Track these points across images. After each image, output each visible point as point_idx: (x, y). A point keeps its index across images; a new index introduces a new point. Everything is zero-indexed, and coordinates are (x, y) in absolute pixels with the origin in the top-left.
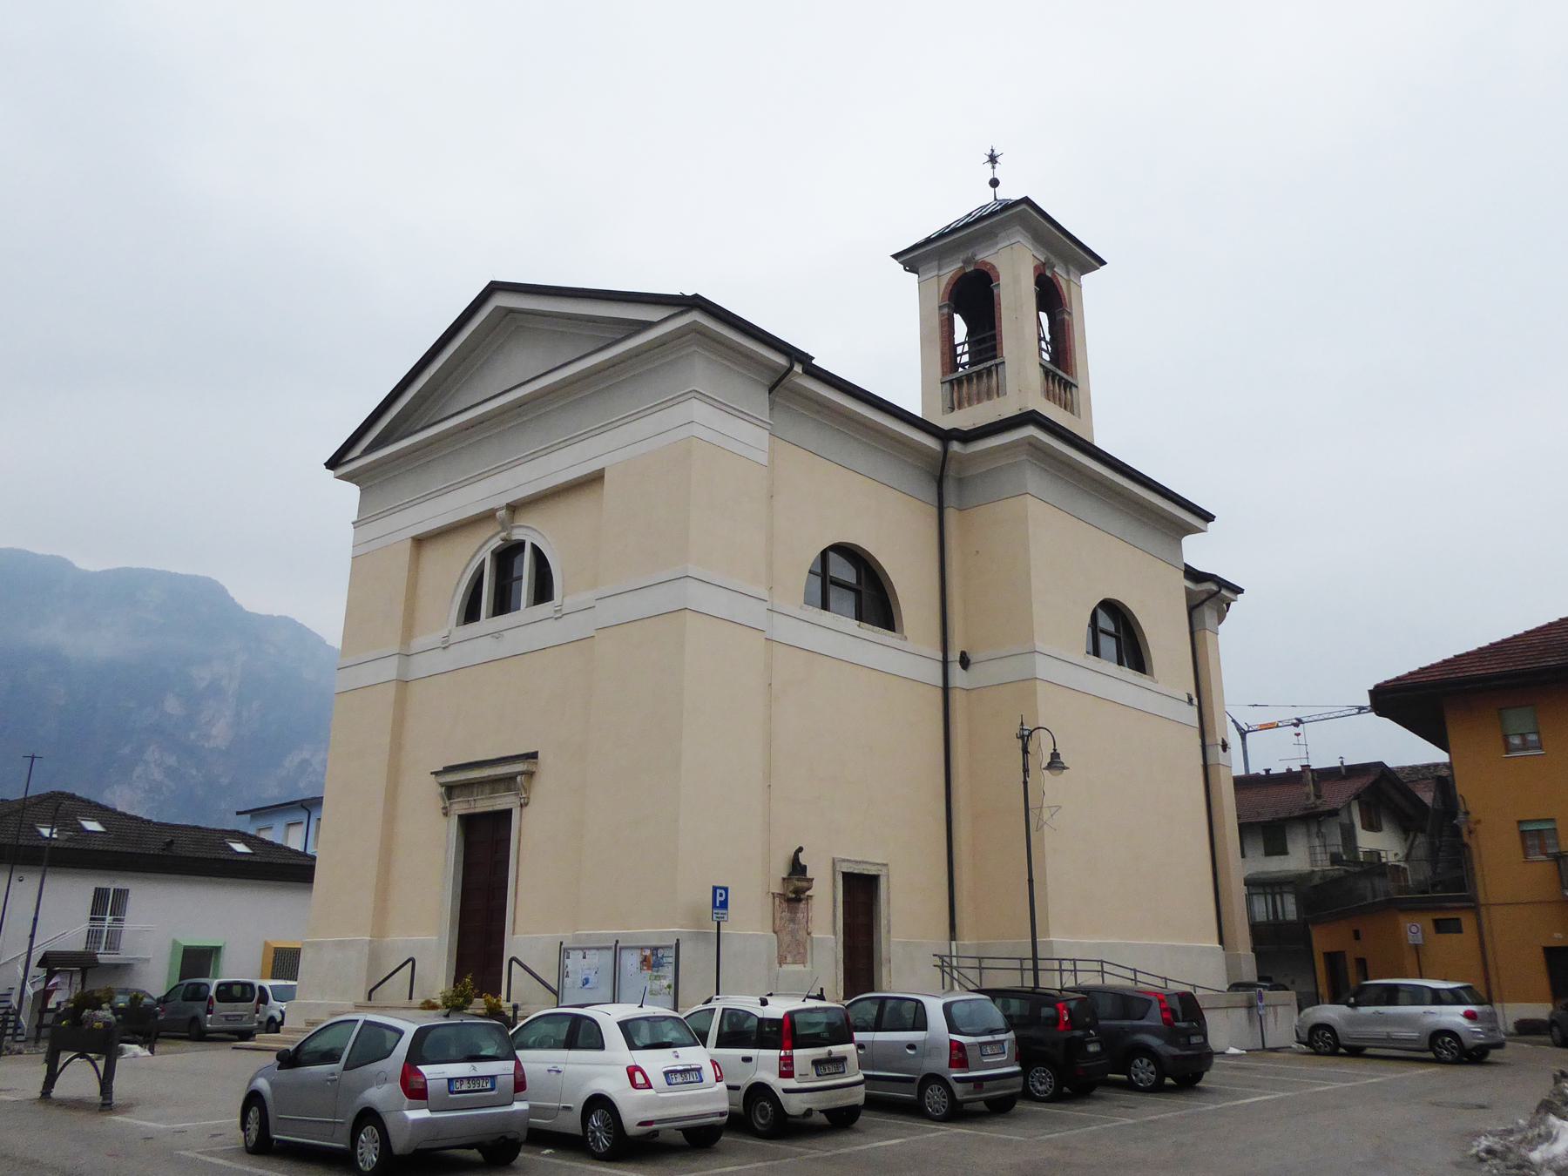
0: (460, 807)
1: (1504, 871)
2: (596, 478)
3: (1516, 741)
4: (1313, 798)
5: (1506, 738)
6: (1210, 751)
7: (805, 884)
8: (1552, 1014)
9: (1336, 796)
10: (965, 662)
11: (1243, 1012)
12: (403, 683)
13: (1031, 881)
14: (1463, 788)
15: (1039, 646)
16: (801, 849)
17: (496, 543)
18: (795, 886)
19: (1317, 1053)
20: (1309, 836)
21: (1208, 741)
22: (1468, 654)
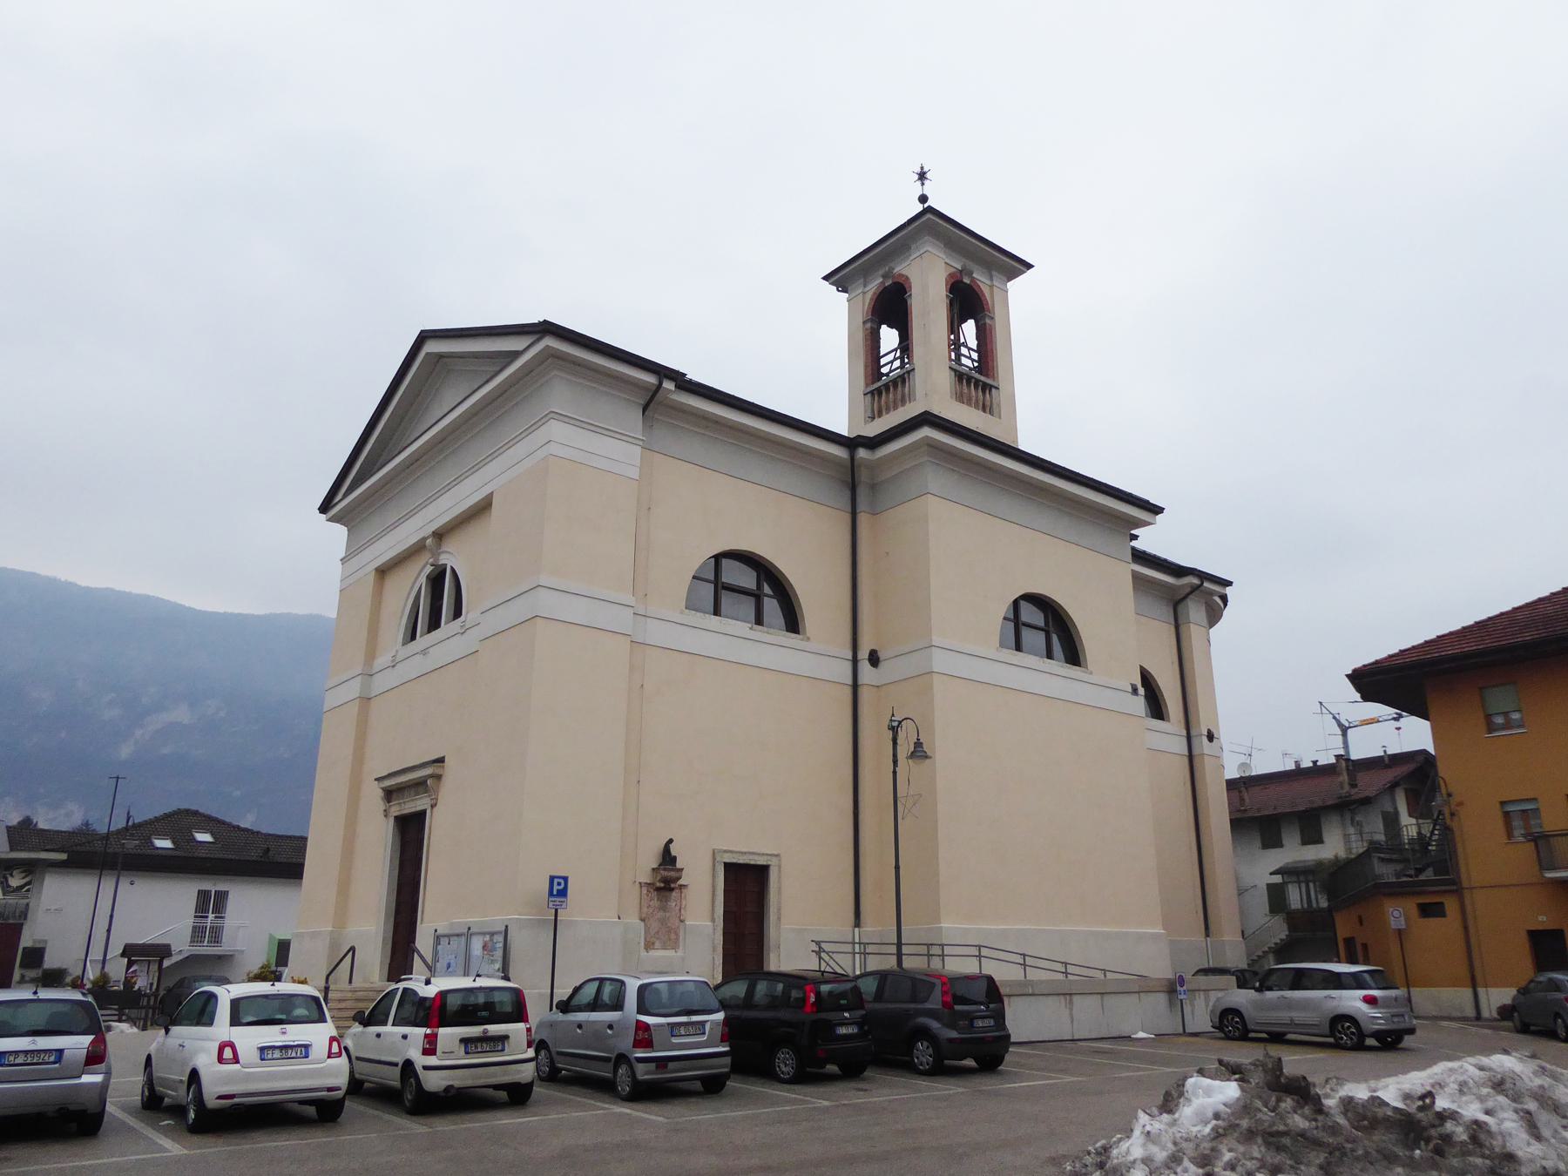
0: (396, 810)
1: (1488, 855)
2: (482, 508)
3: (1499, 720)
4: (1347, 787)
5: (1488, 717)
6: (1195, 742)
7: (673, 874)
8: (1514, 999)
9: (1370, 784)
10: (874, 659)
11: (1162, 999)
12: (365, 700)
13: (897, 868)
14: (1443, 770)
15: (936, 640)
16: (671, 841)
17: (429, 569)
18: (666, 878)
19: (1228, 1038)
20: (1344, 826)
21: (1193, 733)
22: (1451, 633)
